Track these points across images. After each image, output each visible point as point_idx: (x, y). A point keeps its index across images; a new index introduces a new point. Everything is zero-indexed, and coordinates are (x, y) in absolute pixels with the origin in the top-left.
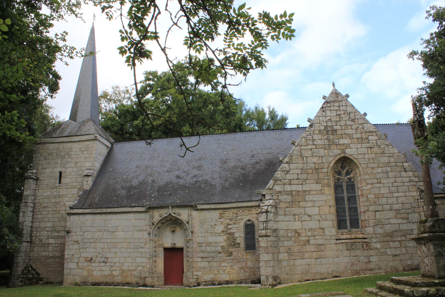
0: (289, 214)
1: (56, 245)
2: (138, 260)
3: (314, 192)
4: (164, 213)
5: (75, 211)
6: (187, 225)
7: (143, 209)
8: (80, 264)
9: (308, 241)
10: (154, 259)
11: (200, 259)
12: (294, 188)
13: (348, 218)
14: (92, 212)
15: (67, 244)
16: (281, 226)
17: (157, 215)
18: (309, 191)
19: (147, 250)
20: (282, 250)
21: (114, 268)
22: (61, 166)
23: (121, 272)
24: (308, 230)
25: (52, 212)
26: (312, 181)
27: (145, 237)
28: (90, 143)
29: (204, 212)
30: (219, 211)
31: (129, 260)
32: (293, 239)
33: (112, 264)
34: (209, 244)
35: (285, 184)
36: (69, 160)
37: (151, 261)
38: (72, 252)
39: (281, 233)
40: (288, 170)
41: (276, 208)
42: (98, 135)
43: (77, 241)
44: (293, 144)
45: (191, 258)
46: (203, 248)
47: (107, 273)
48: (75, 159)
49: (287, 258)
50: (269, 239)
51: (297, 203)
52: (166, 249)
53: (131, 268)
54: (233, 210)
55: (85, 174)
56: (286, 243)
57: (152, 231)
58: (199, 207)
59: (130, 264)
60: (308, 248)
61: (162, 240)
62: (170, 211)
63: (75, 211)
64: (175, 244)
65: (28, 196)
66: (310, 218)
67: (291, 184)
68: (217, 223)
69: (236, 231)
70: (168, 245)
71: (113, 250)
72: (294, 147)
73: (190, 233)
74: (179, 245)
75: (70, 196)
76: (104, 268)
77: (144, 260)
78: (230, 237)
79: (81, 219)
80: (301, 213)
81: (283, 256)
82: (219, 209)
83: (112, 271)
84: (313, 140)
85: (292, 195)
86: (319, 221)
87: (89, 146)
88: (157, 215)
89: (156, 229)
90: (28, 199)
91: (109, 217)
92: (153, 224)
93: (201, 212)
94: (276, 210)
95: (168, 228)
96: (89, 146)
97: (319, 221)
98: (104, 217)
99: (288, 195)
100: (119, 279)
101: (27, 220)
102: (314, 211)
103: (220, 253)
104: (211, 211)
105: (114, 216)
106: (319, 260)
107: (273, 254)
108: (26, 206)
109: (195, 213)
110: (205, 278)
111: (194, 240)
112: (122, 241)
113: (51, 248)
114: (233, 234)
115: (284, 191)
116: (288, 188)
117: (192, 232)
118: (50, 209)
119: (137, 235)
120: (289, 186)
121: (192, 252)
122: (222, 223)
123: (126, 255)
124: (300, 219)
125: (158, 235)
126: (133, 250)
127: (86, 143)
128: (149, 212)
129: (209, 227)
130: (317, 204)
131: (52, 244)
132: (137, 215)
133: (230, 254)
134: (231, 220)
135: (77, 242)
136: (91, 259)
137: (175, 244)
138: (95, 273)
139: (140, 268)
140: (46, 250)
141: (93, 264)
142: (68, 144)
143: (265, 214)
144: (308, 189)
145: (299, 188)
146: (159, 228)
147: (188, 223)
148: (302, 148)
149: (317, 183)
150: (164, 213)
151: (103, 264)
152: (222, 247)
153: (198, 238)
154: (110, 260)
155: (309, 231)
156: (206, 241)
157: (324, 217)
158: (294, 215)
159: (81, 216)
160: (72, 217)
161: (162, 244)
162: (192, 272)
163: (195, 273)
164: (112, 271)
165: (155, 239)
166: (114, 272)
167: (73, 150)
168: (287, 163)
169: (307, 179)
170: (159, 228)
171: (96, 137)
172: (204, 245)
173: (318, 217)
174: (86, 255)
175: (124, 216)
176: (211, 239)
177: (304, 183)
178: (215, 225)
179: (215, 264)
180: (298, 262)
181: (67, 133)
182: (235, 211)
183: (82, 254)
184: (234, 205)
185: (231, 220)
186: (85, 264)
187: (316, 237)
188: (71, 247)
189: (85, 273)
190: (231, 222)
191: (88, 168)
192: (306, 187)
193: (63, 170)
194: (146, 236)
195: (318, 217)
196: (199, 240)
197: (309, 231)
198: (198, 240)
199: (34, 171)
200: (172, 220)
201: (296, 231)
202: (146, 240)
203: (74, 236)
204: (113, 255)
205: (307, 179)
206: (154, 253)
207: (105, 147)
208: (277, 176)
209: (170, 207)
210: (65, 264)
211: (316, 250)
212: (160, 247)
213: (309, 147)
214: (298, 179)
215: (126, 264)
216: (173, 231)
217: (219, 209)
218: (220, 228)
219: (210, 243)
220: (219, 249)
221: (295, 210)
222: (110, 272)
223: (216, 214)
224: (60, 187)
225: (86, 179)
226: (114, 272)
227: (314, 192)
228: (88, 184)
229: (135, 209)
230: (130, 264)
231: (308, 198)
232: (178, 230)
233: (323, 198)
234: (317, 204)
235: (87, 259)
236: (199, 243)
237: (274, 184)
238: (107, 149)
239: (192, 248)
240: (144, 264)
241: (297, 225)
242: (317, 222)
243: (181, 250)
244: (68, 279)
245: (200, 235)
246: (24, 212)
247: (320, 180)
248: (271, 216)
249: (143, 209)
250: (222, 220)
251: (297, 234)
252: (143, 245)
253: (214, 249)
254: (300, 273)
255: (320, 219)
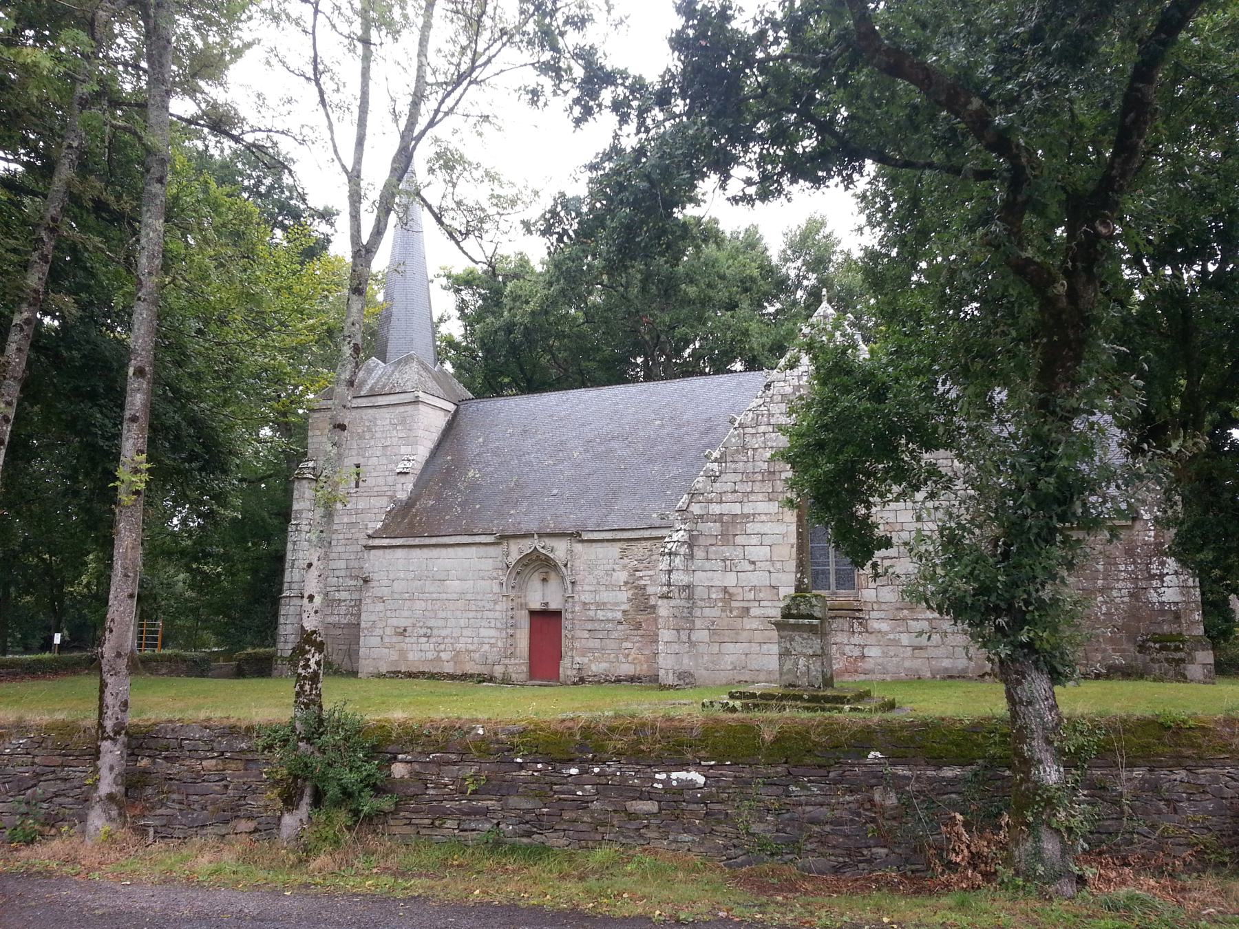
0: (714, 557)
1: (353, 603)
2: (484, 632)
3: (764, 518)
4: (527, 546)
5: (377, 542)
6: (563, 569)
7: (490, 539)
8: (386, 640)
9: (748, 609)
10: (510, 631)
11: (586, 634)
12: (725, 508)
13: (832, 568)
14: (406, 543)
15: (363, 602)
16: (700, 578)
17: (516, 550)
18: (754, 515)
19: (497, 615)
20: (698, 623)
21: (442, 647)
22: (358, 455)
23: (455, 656)
24: (747, 589)
25: (343, 542)
26: (760, 497)
27: (494, 591)
28: (409, 408)
29: (594, 545)
30: (619, 545)
31: (466, 632)
32: (720, 604)
33: (439, 640)
34: (601, 606)
35: (711, 501)
36: (372, 443)
37: (504, 635)
38: (373, 618)
39: (699, 593)
40: (717, 474)
41: (691, 546)
42: (421, 394)
43: (382, 598)
44: (732, 421)
45: (570, 631)
46: (592, 613)
47: (430, 656)
48: (383, 441)
49: (707, 639)
50: (672, 603)
51: (731, 538)
52: (533, 613)
53: (471, 647)
54: (644, 543)
55: (398, 471)
56: (707, 612)
57: (505, 579)
58: (585, 536)
59: (470, 641)
60: (750, 624)
61: (525, 596)
62: (536, 543)
63: (377, 542)
64: (547, 604)
65: (300, 512)
66: (751, 567)
67: (721, 502)
68: (616, 567)
69: (649, 582)
70: (536, 606)
71: (441, 614)
72: (732, 430)
73: (570, 586)
74: (553, 606)
75: (376, 511)
76: (425, 647)
77: (493, 633)
78: (637, 594)
79: (388, 557)
80: (737, 556)
81: (701, 635)
82: (620, 540)
83: (439, 652)
84: (770, 415)
85: (722, 522)
86: (770, 572)
87: (405, 414)
88: (516, 550)
89: (514, 575)
90: (300, 518)
91: (435, 552)
92: (508, 567)
93: (589, 544)
94: (692, 550)
95: (536, 574)
96: (405, 414)
97: (770, 572)
98: (426, 553)
99: (715, 522)
100: (449, 668)
101: (301, 557)
102: (760, 553)
103: (620, 623)
104: (606, 544)
105: (444, 551)
106: (765, 646)
107: (678, 630)
108: (297, 530)
109: (578, 547)
110: (594, 668)
111: (577, 597)
112: (455, 596)
113: (343, 610)
114: (644, 588)
115: (708, 514)
116: (715, 509)
117: (573, 583)
118: (341, 537)
119: (486, 584)
120: (718, 506)
121: (573, 619)
122: (625, 567)
123: (462, 622)
124: (734, 569)
125: (517, 586)
126: (474, 613)
127: (401, 409)
128: (501, 543)
129: (602, 573)
130: (767, 541)
131: (345, 601)
132: (482, 550)
133: (638, 626)
134: (640, 561)
135: (381, 599)
136: (405, 630)
137: (547, 604)
138: (411, 656)
139: (486, 647)
140: (336, 612)
141: (407, 640)
142: (370, 411)
143: (667, 557)
144: (752, 512)
145: (736, 508)
146: (518, 573)
147: (566, 565)
148: (747, 430)
149: (770, 500)
150: (527, 546)
151: (424, 640)
152: (624, 611)
153: (584, 595)
154: (435, 632)
155: (750, 590)
156: (597, 599)
157: (778, 565)
158: (724, 560)
159: (387, 551)
160: (373, 552)
161: (526, 604)
162: (572, 657)
163: (577, 659)
164: (439, 652)
165: (512, 594)
166: (442, 654)
167: (379, 422)
168: (716, 460)
169: (752, 492)
170: (518, 573)
171: (418, 397)
172: (593, 607)
173: (768, 566)
174: (395, 622)
175: (459, 550)
176: (605, 596)
177: (746, 500)
178: (614, 570)
179: (612, 644)
180: (730, 647)
181: (368, 388)
182: (648, 544)
183: (389, 621)
184: (647, 534)
185: (640, 561)
186: (394, 639)
187: (762, 603)
188: (371, 608)
189: (394, 656)
190: (641, 567)
191: (405, 458)
192: (748, 509)
193: (361, 461)
194: (496, 589)
195: (768, 566)
196: (586, 597)
197: (750, 590)
198: (583, 598)
199: (311, 464)
200: (541, 560)
201: (725, 590)
202: (496, 597)
203: (376, 589)
204: (441, 623)
205: (752, 492)
206: (510, 621)
207: (442, 413)
208: (697, 487)
209: (536, 536)
210: (362, 639)
211: (761, 627)
212: (521, 609)
213: (762, 429)
214: (735, 491)
215: (462, 640)
216: (544, 580)
217: (620, 540)
218: (622, 576)
219: (604, 604)
220: (619, 615)
221: (727, 552)
222: (436, 654)
223: (614, 550)
224: (359, 494)
225: (402, 479)
226: (442, 654)
227: (764, 518)
228: (405, 489)
229: (477, 539)
230: (470, 641)
231: (751, 528)
232: (553, 575)
233: (779, 529)
234: (767, 541)
235: (398, 630)
236: (585, 604)
237: (690, 502)
238: (446, 416)
239: (573, 612)
240: (493, 641)
241: (730, 580)
242: (767, 574)
243: (557, 614)
244: (365, 666)
245: (586, 588)
246: (294, 543)
247: (775, 494)
248: (678, 561)
249: (490, 539)
250: (626, 560)
251: (727, 597)
252: (489, 606)
253: (610, 615)
254: (729, 668)
255: (772, 570)
